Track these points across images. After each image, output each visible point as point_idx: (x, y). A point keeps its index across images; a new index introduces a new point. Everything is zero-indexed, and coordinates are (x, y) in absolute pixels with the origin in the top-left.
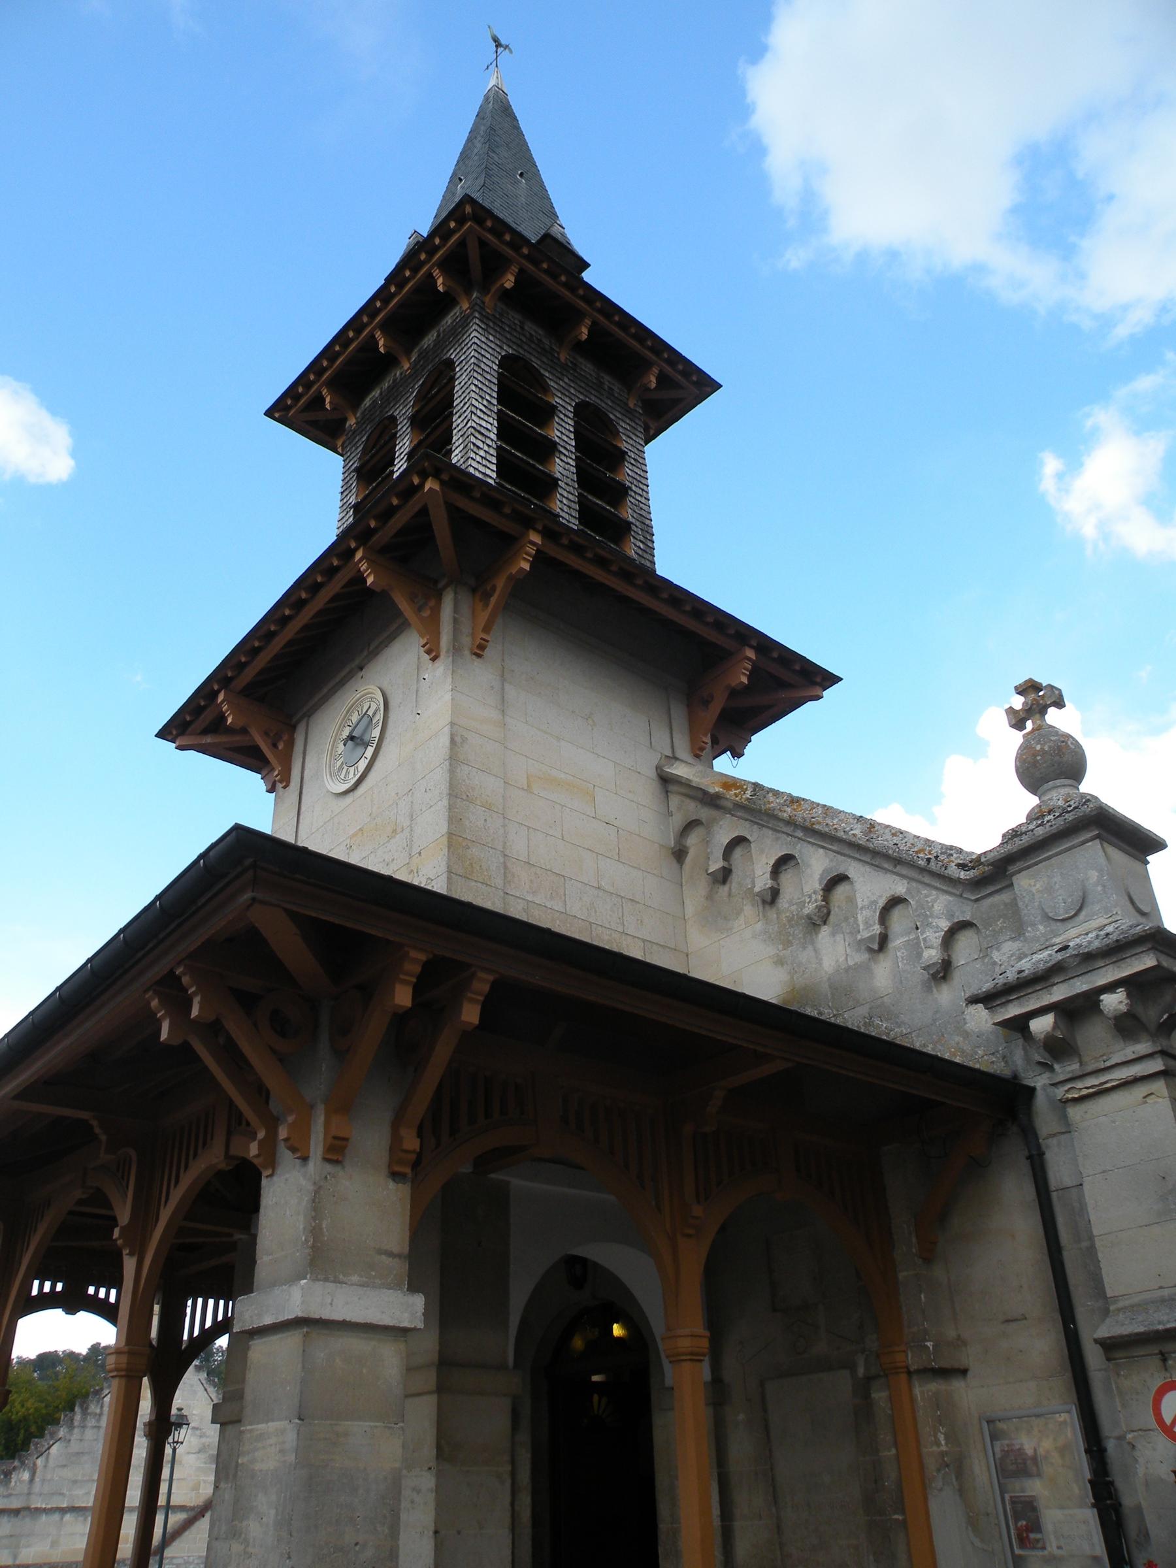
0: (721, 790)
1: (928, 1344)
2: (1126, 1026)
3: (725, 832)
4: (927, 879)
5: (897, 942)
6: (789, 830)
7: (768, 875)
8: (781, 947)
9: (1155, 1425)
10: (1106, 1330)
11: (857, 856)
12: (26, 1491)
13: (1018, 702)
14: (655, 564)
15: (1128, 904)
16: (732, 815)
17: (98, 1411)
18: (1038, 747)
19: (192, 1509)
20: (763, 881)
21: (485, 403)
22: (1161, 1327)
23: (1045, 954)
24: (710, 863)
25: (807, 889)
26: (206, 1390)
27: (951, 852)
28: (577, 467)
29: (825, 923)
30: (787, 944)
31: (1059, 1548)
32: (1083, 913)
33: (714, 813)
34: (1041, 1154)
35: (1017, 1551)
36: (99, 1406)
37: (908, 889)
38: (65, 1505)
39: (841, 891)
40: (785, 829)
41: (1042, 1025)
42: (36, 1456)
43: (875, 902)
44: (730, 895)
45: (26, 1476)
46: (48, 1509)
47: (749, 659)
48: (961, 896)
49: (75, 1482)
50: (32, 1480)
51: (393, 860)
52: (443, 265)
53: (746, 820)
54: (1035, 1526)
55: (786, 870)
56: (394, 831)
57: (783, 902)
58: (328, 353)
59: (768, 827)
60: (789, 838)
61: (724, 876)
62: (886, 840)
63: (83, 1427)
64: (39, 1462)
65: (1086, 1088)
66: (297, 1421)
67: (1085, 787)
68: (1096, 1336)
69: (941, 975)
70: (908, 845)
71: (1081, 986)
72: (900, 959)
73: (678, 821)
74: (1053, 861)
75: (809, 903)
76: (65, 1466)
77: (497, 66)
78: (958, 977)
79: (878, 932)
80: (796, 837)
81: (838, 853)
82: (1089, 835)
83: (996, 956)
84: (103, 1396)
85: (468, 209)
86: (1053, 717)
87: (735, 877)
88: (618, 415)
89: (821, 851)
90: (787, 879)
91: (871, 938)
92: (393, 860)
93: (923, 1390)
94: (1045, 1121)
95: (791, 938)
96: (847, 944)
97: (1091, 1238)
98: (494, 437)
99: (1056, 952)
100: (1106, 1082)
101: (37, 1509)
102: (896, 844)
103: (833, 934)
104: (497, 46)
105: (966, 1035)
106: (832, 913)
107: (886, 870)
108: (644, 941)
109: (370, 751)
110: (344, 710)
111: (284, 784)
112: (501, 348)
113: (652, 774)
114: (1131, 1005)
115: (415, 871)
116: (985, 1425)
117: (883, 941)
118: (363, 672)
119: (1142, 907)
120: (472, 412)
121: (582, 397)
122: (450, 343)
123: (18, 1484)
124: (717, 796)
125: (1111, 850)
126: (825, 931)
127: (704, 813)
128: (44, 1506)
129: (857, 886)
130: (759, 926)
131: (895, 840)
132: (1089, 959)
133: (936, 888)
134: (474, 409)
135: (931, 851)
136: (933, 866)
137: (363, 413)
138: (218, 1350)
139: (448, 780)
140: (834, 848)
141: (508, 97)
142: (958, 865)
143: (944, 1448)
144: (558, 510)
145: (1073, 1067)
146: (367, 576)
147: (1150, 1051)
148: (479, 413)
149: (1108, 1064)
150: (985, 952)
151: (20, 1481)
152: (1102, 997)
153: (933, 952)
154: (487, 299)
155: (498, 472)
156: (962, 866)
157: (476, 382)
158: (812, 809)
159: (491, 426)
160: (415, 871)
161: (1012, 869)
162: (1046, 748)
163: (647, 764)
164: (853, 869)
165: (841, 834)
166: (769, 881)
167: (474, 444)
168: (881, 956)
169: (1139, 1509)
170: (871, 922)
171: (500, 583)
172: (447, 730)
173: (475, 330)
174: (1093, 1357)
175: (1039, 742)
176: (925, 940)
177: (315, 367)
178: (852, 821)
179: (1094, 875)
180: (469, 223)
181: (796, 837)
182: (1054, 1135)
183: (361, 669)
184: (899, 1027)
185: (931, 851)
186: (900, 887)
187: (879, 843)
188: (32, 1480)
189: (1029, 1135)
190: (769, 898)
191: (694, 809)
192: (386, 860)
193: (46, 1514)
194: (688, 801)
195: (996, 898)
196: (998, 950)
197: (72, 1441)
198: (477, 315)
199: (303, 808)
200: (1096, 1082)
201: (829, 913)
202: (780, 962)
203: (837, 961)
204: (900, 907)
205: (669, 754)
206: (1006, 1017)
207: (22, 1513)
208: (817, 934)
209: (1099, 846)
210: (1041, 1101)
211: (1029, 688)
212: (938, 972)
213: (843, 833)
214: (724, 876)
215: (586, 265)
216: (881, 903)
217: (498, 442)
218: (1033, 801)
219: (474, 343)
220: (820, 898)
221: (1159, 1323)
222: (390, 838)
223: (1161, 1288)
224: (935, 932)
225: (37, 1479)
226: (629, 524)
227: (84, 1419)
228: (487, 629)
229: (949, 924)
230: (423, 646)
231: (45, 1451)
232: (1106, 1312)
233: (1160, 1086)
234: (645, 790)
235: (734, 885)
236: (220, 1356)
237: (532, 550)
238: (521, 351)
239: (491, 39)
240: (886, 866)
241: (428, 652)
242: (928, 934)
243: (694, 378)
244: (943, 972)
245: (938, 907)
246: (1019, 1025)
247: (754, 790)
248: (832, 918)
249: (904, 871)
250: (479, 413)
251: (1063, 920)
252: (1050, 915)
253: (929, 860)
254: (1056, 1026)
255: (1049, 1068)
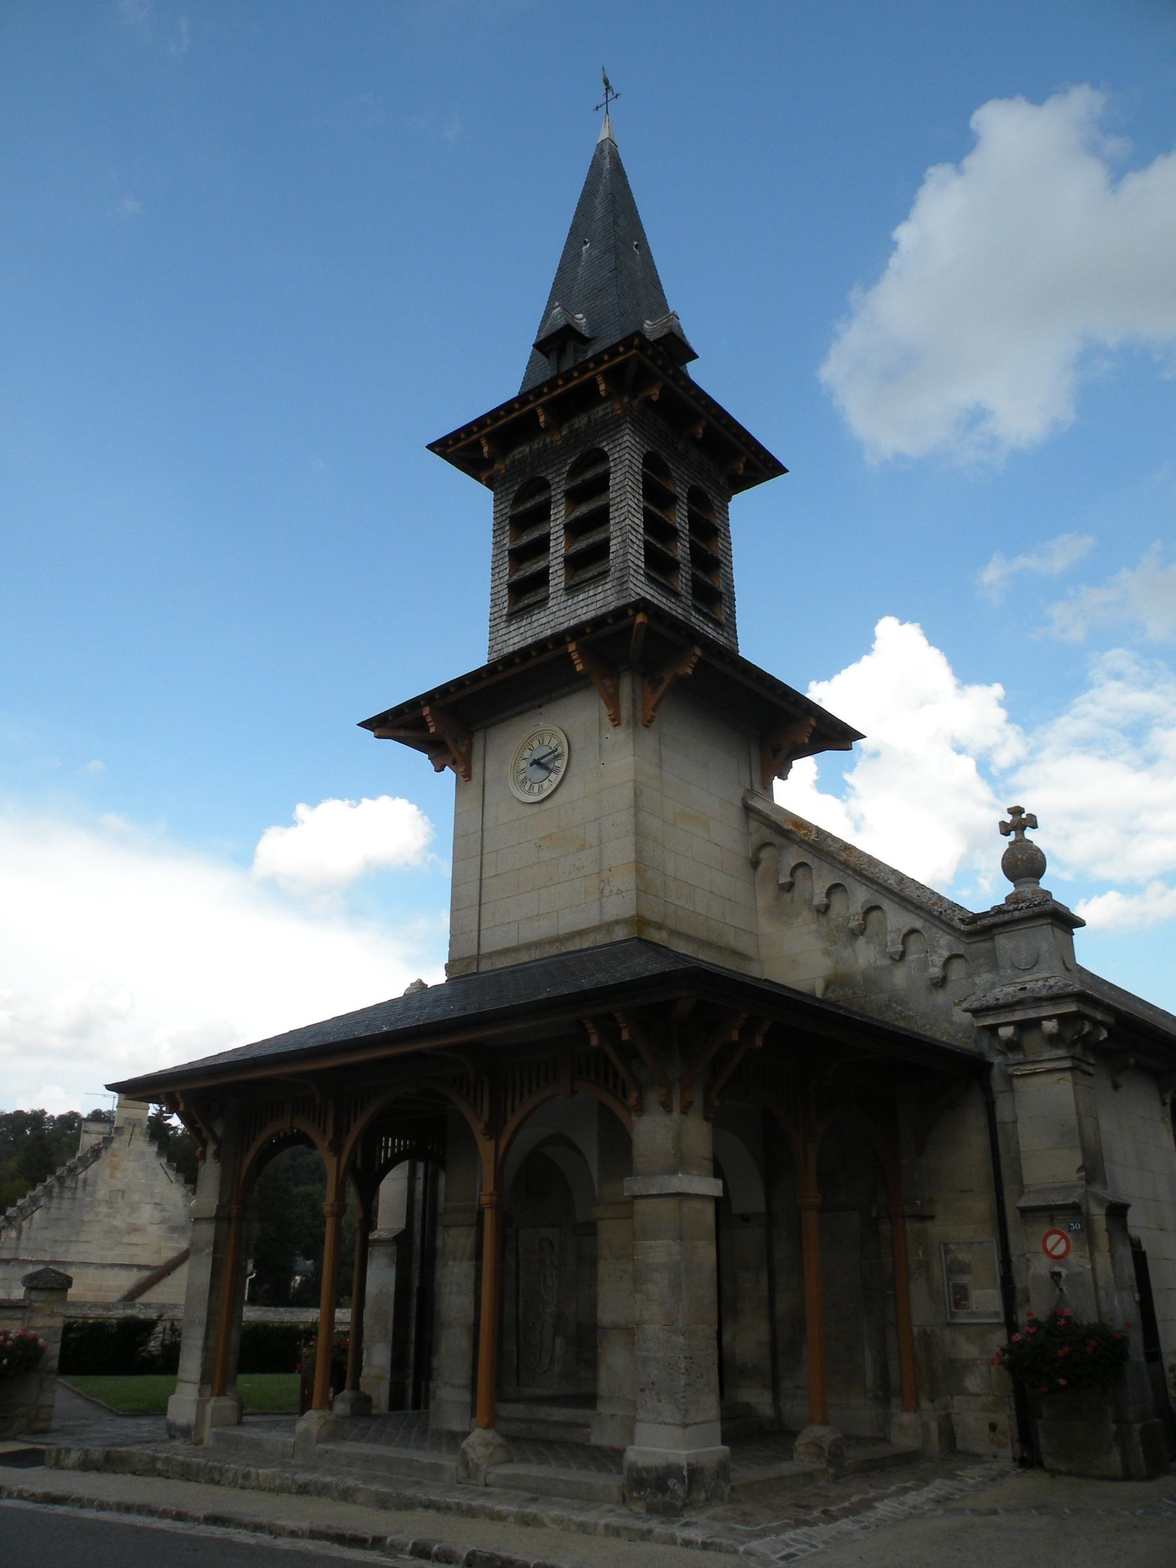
0: (793, 828)
1: (918, 1202)
2: (1054, 1040)
3: (793, 856)
4: (937, 923)
5: (911, 957)
6: (842, 867)
7: (824, 895)
8: (828, 944)
9: (1041, 1250)
10: (1023, 1202)
11: (891, 897)
12: (14, 1246)
13: (1008, 819)
14: (736, 625)
15: (1062, 965)
16: (799, 846)
17: (73, 1185)
18: (1020, 856)
19: (155, 1268)
20: (820, 899)
21: (636, 501)
22: (1053, 1203)
23: (1011, 989)
24: (780, 876)
25: (852, 910)
26: (166, 1173)
27: (955, 909)
28: (690, 548)
29: (862, 934)
30: (834, 943)
31: (977, 1308)
32: (1036, 968)
33: (784, 841)
34: (994, 1102)
35: (953, 1310)
36: (74, 1181)
37: (923, 927)
38: (48, 1259)
39: (875, 915)
40: (839, 866)
41: (1006, 1032)
42: (21, 1219)
43: (900, 930)
44: (792, 900)
45: (13, 1234)
46: (34, 1261)
47: (811, 725)
48: (959, 938)
49: (55, 1241)
50: (19, 1237)
51: (583, 867)
52: (606, 375)
53: (810, 852)
54: (965, 1297)
55: (836, 892)
56: (583, 846)
57: (833, 913)
58: (494, 415)
59: (826, 862)
60: (841, 873)
61: (790, 887)
62: (912, 891)
63: (60, 1198)
64: (25, 1224)
65: (1027, 1070)
66: (679, 1241)
67: (1044, 883)
68: (1018, 1205)
69: (939, 984)
70: (927, 898)
71: (1032, 1014)
72: (912, 968)
73: (755, 839)
74: (1021, 931)
75: (853, 920)
76: (46, 1228)
77: (607, 113)
78: (950, 987)
79: (901, 950)
80: (846, 873)
81: (876, 891)
82: (1045, 921)
83: (977, 980)
84: (77, 1173)
85: (636, 342)
86: (1029, 834)
87: (796, 888)
88: (714, 495)
89: (865, 887)
90: (837, 901)
91: (895, 953)
92: (583, 867)
93: (911, 1227)
94: (997, 1084)
95: (836, 939)
96: (876, 951)
97: (1018, 1152)
98: (641, 531)
99: (1019, 990)
100: (1038, 1069)
101: (24, 1260)
102: (918, 896)
103: (868, 943)
104: (607, 89)
105: (952, 1023)
106: (868, 928)
107: (909, 911)
108: (735, 928)
109: (555, 778)
110: (526, 736)
111: (466, 779)
112: (643, 447)
113: (739, 803)
114: (1059, 1030)
115: (606, 881)
116: (942, 1246)
117: (903, 955)
118: (541, 710)
119: (1068, 966)
120: (629, 511)
121: (692, 482)
122: (603, 434)
123: (7, 1240)
124: (790, 831)
125: (1056, 930)
126: (861, 940)
127: (776, 839)
128: (30, 1259)
129: (889, 916)
130: (814, 927)
131: (918, 892)
132: (1038, 1001)
133: (943, 930)
134: (630, 509)
135: (941, 905)
136: (943, 917)
137: (513, 462)
138: (48, 1119)
139: (634, 823)
140: (875, 888)
141: (618, 149)
142: (960, 919)
143: (921, 1258)
144: (680, 589)
145: (1020, 1057)
146: (577, 664)
147: (1064, 1055)
148: (632, 511)
149: (1040, 1059)
150: (970, 976)
151: (8, 1237)
152: (1043, 1022)
153: (937, 970)
154: (635, 403)
155: (646, 563)
156: (962, 921)
157: (630, 484)
158: (859, 857)
159: (639, 520)
160: (606, 881)
161: (996, 931)
162: (1024, 858)
163: (735, 795)
164: (886, 905)
165: (881, 881)
166: (825, 899)
167: (631, 540)
168: (900, 964)
169: (1026, 1290)
170: (896, 942)
171: (668, 678)
172: (631, 784)
173: (628, 434)
174: (1011, 1215)
175: (1020, 853)
176: (932, 961)
177: (480, 422)
178: (888, 872)
179: (1045, 946)
180: (634, 351)
181: (846, 873)
182: (1001, 1092)
183: (540, 707)
184: (908, 1011)
185: (941, 905)
186: (918, 924)
187: (908, 892)
188: (19, 1237)
189: (987, 1090)
190: (823, 910)
191: (767, 834)
192: (576, 865)
193: (33, 1265)
194: (764, 828)
195: (981, 945)
196: (979, 977)
197: (52, 1209)
198: (628, 419)
199: (487, 803)
200: (1032, 1067)
201: (865, 928)
202: (827, 953)
203: (869, 961)
204: (916, 934)
205: (749, 788)
206: (986, 1024)
207: (12, 1263)
208: (856, 940)
209: (1051, 929)
210: (996, 1072)
211: (1016, 811)
212: (938, 983)
213: (883, 881)
214: (790, 887)
215: (693, 356)
216: (904, 931)
217: (645, 536)
218: (1009, 888)
219: (628, 447)
220: (861, 918)
221: (1053, 1201)
222: (579, 850)
223: (1054, 1182)
224: (939, 957)
225: (23, 1237)
226: (721, 594)
227: (61, 1192)
228: (654, 709)
229: (949, 954)
230: (610, 716)
231: (29, 1215)
232: (1021, 1193)
233: (1068, 1075)
234: (734, 814)
235: (796, 894)
236: (51, 1126)
237: (695, 660)
238: (656, 448)
239: (602, 81)
240: (910, 908)
241: (613, 720)
242: (934, 957)
243: (762, 457)
244: (940, 983)
245: (942, 942)
246: (993, 1029)
247: (817, 833)
248: (867, 932)
249: (922, 914)
250: (632, 511)
251: (1024, 970)
252: (1016, 965)
253: (941, 912)
254: (1014, 1034)
255: (1005, 1054)
